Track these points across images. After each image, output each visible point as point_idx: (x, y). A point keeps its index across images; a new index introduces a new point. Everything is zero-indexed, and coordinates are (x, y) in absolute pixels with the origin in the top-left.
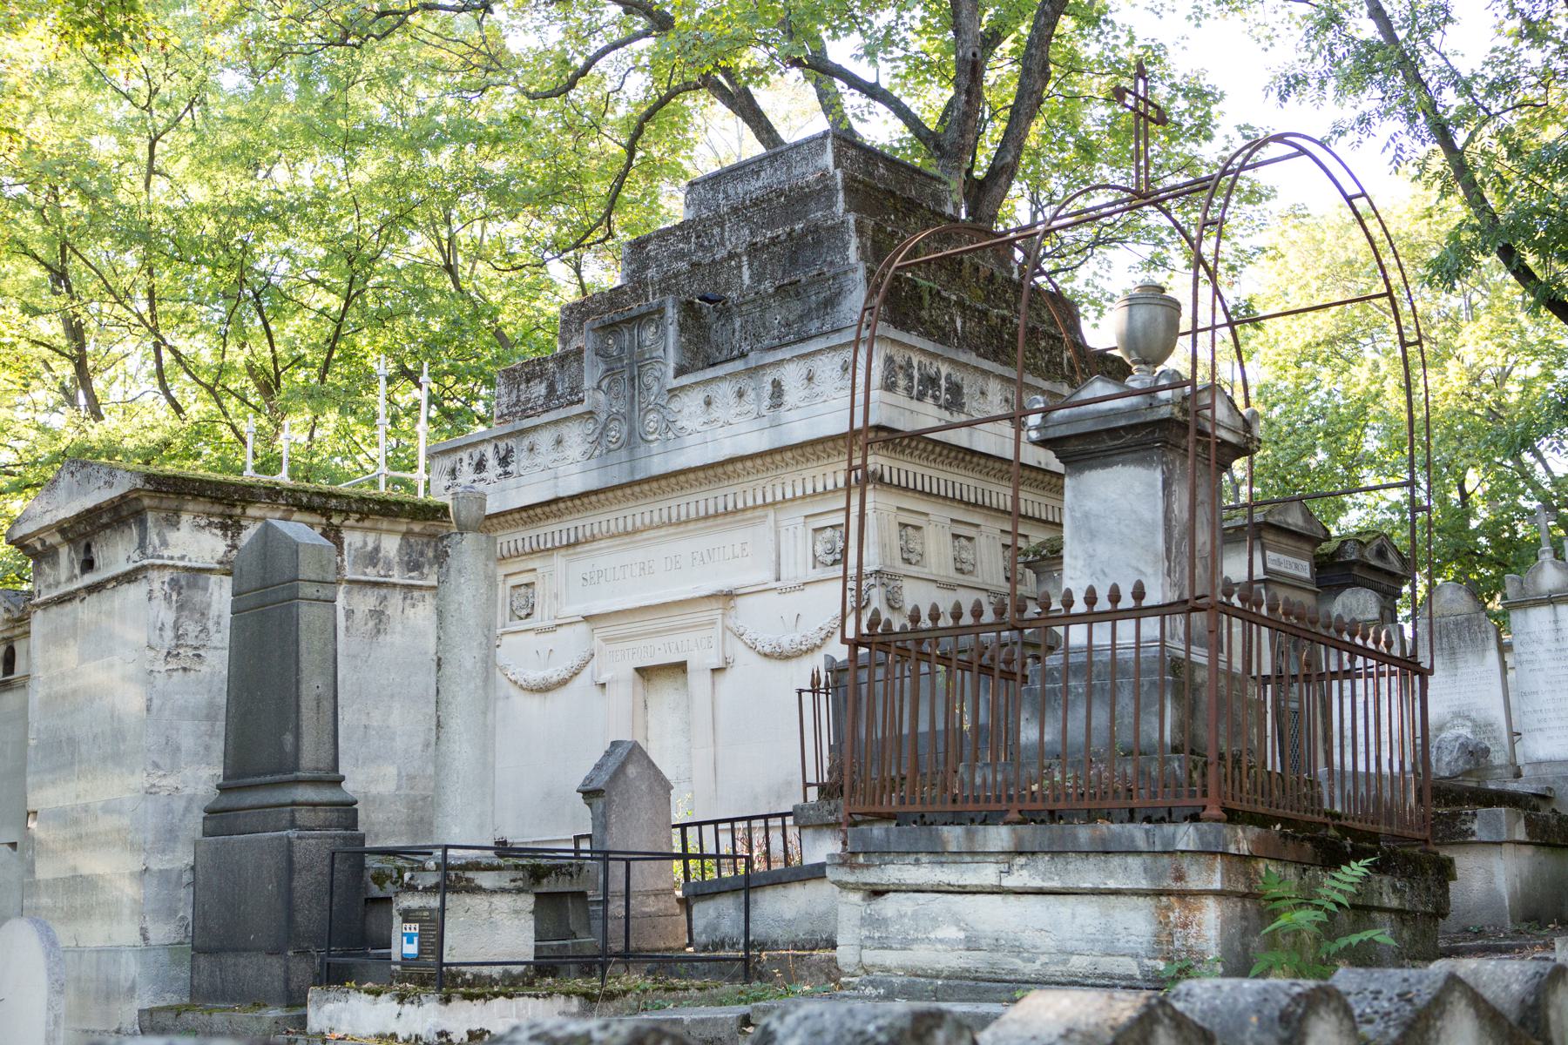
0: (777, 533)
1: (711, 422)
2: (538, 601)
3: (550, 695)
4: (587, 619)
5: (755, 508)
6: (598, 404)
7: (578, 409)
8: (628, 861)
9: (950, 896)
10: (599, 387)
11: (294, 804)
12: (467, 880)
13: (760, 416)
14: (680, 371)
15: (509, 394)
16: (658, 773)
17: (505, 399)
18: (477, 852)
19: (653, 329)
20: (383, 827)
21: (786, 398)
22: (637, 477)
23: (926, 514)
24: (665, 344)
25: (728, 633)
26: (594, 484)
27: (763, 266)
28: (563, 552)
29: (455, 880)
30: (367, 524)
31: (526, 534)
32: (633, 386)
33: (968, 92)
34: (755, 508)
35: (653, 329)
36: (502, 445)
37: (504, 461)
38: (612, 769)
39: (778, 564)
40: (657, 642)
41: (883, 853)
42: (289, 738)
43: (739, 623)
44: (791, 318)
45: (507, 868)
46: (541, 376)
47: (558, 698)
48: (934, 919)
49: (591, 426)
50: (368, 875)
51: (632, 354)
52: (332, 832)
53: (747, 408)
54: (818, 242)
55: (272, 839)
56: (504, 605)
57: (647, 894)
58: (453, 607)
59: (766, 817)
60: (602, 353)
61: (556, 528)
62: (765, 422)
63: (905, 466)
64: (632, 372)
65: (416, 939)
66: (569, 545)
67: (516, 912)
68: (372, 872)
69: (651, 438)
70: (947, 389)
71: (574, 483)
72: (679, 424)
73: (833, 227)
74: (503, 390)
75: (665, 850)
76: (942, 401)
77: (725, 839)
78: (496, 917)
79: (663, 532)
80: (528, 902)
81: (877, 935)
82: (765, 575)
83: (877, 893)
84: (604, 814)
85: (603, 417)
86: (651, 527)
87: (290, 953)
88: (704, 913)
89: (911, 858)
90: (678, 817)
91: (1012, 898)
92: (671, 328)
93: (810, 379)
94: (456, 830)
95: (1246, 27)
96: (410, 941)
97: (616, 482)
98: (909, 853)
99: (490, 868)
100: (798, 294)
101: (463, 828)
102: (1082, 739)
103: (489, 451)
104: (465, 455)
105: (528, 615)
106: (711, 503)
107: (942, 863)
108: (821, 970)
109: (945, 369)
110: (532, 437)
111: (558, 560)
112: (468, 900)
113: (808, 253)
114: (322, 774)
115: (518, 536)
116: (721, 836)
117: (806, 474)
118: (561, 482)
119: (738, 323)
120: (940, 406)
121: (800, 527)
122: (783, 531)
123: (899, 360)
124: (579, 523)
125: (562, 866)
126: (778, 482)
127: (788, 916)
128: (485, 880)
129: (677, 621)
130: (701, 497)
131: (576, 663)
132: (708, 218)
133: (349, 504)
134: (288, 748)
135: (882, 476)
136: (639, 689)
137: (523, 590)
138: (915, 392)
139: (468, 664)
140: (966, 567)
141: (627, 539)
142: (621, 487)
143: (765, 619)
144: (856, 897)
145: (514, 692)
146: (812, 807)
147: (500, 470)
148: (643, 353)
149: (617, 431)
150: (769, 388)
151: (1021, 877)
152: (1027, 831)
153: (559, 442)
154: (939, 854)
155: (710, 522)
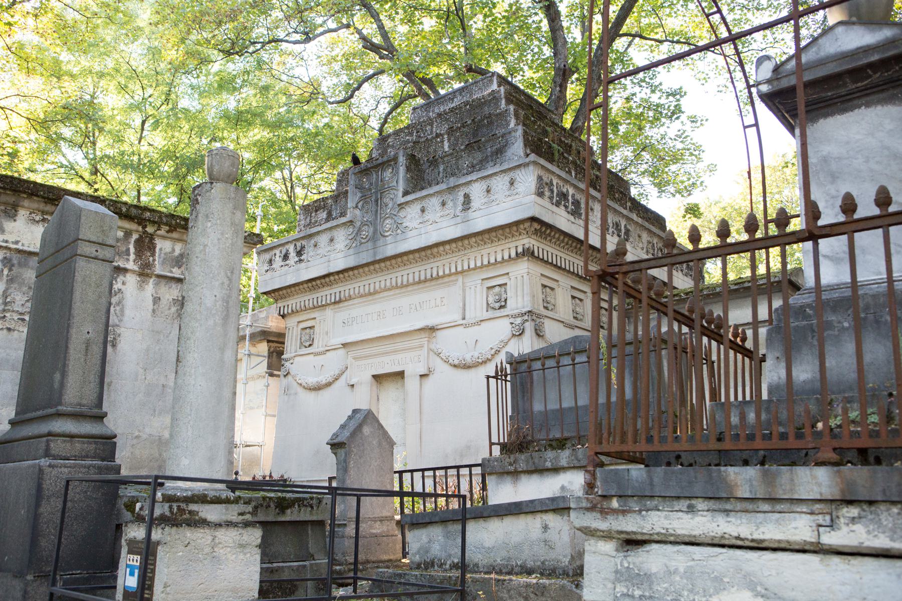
0: (464, 291)
1: (425, 222)
2: (316, 337)
3: (321, 392)
4: (344, 345)
5: (450, 275)
6: (356, 216)
7: (343, 220)
8: (359, 498)
9: (739, 552)
10: (357, 207)
11: (50, 434)
12: (190, 512)
13: (455, 216)
14: (406, 193)
15: (305, 219)
16: (385, 433)
17: (303, 222)
18: (206, 485)
19: (390, 170)
20: (129, 460)
21: (472, 204)
22: (378, 258)
23: (557, 281)
24: (397, 179)
25: (431, 353)
26: (351, 262)
27: (457, 140)
28: (332, 307)
29: (183, 514)
30: (175, 235)
31: (310, 297)
32: (377, 205)
33: (561, 86)
34: (450, 275)
35: (390, 170)
36: (299, 244)
37: (299, 253)
38: (352, 429)
39: (464, 309)
40: (386, 359)
41: (646, 497)
42: (57, 376)
43: (438, 346)
44: (475, 162)
45: (237, 501)
46: (324, 207)
47: (326, 394)
48: (718, 580)
49: (351, 230)
50: (121, 504)
51: (377, 185)
52: (88, 462)
53: (448, 212)
54: (491, 123)
55: (29, 467)
56: (296, 340)
57: (374, 520)
58: (199, 248)
59: (458, 467)
60: (359, 187)
61: (328, 293)
62: (459, 220)
63: (547, 248)
64: (377, 197)
65: (137, 571)
66: (335, 303)
67: (242, 546)
68: (125, 500)
69: (386, 234)
70: (572, 203)
71: (340, 264)
72: (404, 225)
73: (500, 114)
74: (302, 217)
75: (389, 488)
76: (569, 210)
77: (452, 481)
78: (220, 551)
79: (392, 293)
80: (255, 535)
81: (637, 593)
82: (456, 317)
83: (632, 543)
84: (345, 461)
85: (358, 224)
86: (386, 289)
87: (30, 577)
88: (417, 539)
89: (683, 504)
90: (398, 467)
91: (836, 559)
92: (401, 168)
93: (488, 191)
94: (185, 462)
95: (693, 73)
96: (132, 574)
97: (364, 262)
98: (684, 498)
99: (217, 501)
100: (479, 148)
101: (192, 463)
102: (854, 376)
103: (291, 248)
104: (277, 252)
105: (310, 345)
106: (423, 273)
107: (727, 512)
108: (520, 594)
109: (571, 191)
110: (316, 239)
111: (329, 312)
112: (189, 534)
113: (485, 130)
114: (84, 409)
115: (306, 298)
116: (426, 480)
117: (483, 252)
118: (331, 264)
119: (441, 169)
120: (568, 212)
121: (479, 286)
122: (467, 289)
123: (545, 179)
124: (342, 289)
125: (305, 499)
126: (465, 258)
127: (487, 544)
128: (211, 513)
129: (400, 346)
130: (416, 270)
131: (337, 372)
132: (424, 121)
133: (160, 217)
134: (56, 385)
135: (533, 252)
136: (374, 388)
137: (308, 330)
138: (554, 201)
139: (209, 301)
140: (579, 316)
141: (370, 298)
142: (367, 265)
143: (454, 343)
144: (609, 547)
145: (300, 390)
146: (496, 460)
147: (297, 259)
148: (384, 185)
149: (367, 231)
150: (461, 199)
151: (851, 532)
152: (859, 474)
153: (332, 240)
154: (722, 499)
155: (421, 286)
